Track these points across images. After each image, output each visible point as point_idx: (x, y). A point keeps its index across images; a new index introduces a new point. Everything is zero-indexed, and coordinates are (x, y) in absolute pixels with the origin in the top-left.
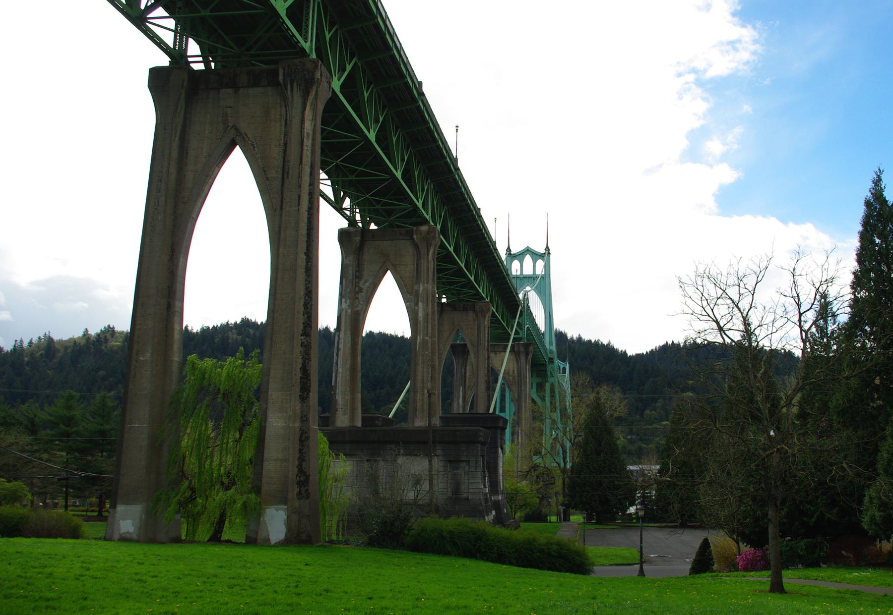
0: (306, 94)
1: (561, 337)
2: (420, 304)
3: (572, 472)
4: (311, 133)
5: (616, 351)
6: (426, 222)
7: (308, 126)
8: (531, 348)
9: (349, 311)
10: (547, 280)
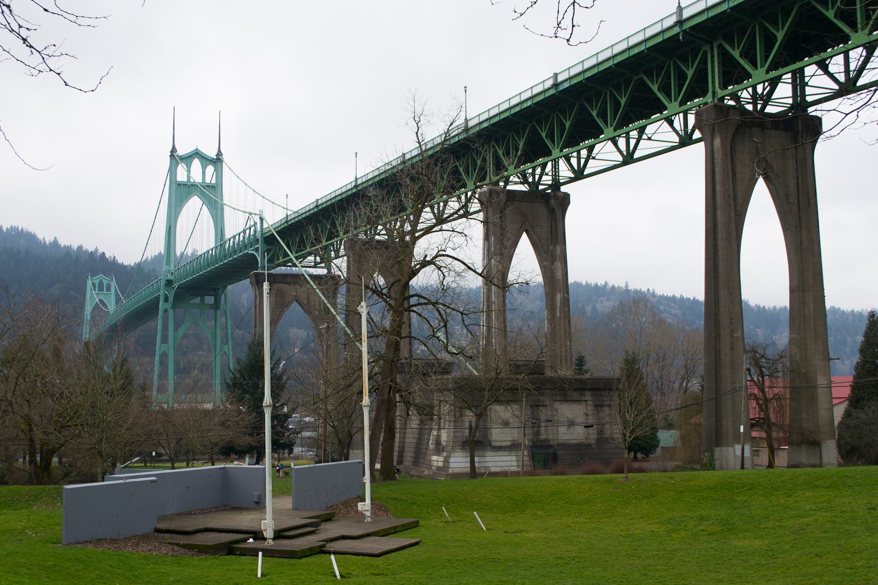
3: (699, 88)
10: (219, 191)
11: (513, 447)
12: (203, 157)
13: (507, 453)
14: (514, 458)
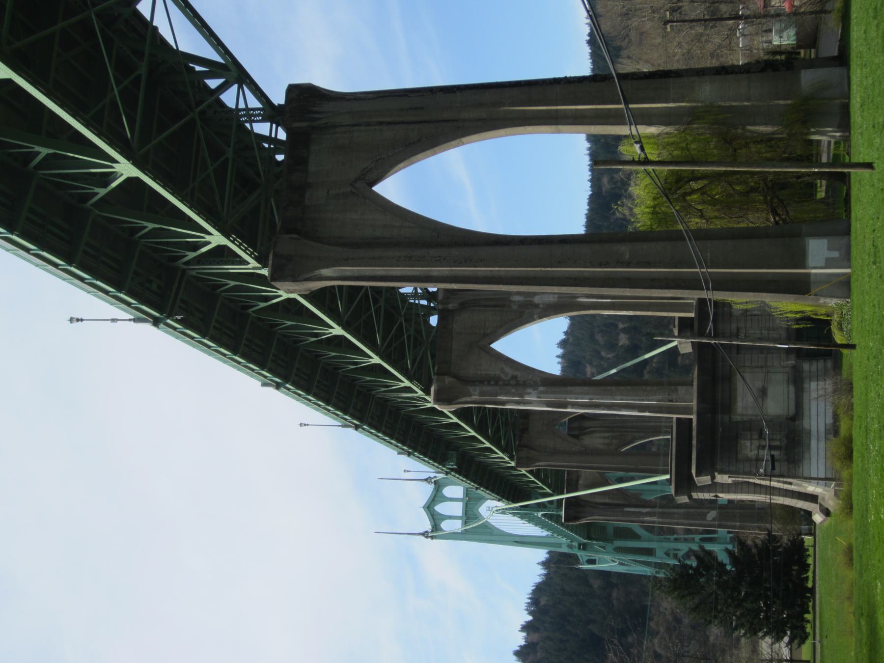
9: (541, 388)
11: (797, 381)
13: (806, 396)
14: (813, 385)
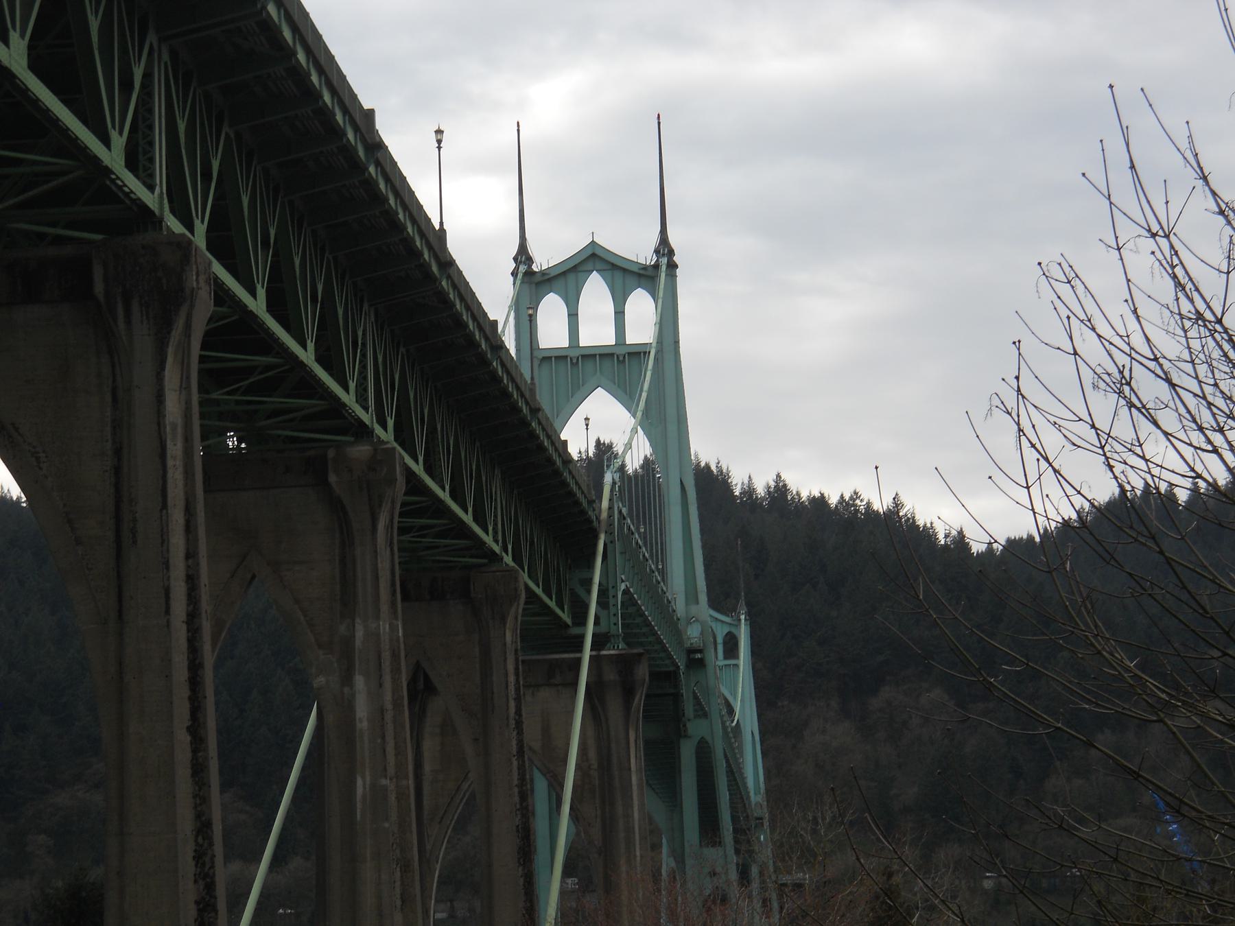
0: (163, 326)
1: (711, 484)
2: (359, 681)
4: (180, 422)
5: (925, 536)
6: (362, 431)
7: (173, 406)
8: (642, 672)
12: (614, 267)
